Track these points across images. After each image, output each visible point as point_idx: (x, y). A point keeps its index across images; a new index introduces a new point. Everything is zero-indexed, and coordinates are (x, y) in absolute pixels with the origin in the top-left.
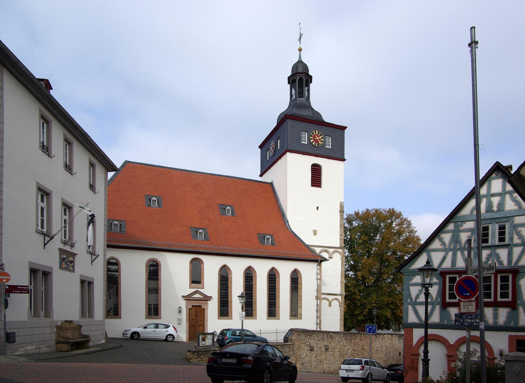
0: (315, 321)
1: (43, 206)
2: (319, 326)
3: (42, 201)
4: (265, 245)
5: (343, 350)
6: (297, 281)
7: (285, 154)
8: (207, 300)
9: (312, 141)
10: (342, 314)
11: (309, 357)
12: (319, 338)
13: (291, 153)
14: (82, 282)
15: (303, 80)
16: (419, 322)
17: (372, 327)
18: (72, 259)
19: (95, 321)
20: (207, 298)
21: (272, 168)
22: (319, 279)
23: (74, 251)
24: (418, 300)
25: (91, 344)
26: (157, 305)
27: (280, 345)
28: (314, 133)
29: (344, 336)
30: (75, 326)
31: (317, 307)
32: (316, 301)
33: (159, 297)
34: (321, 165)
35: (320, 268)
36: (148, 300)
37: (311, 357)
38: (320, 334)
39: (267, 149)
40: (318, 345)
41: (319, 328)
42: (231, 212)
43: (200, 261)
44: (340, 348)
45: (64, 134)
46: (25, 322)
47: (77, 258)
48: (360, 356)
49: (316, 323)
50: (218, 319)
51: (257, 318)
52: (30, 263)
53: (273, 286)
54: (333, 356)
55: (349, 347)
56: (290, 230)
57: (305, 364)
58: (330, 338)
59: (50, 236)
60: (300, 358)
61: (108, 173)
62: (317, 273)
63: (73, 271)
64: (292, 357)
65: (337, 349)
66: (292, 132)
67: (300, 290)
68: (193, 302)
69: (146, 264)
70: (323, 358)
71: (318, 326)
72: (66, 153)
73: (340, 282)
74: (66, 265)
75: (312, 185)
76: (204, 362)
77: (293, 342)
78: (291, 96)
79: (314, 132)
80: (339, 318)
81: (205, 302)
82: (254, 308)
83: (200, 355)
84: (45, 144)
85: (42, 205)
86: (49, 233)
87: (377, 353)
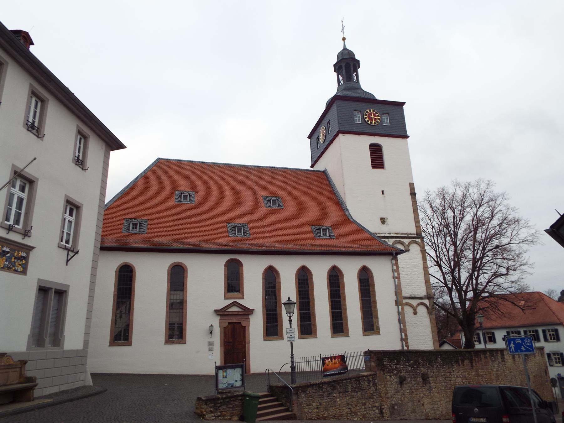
1: (71, 219)
2: (406, 343)
3: (71, 214)
5: (449, 379)
6: (368, 282)
7: (338, 136)
8: (249, 315)
13: (344, 134)
14: (43, 290)
15: (350, 65)
18: (24, 255)
19: (64, 351)
20: (247, 312)
22: (397, 278)
23: (27, 241)
25: (37, 393)
26: (182, 324)
28: (369, 112)
30: (12, 363)
31: (399, 316)
33: (184, 313)
34: (381, 144)
35: (395, 263)
36: (170, 317)
37: (404, 394)
39: (317, 137)
41: (406, 346)
43: (239, 264)
45: (78, 126)
46: (86, 356)
50: (264, 340)
51: (318, 337)
52: (39, 280)
54: (436, 389)
59: (74, 251)
62: (393, 270)
63: (24, 272)
67: (372, 294)
68: (229, 317)
69: (168, 270)
72: (80, 147)
73: (424, 281)
75: (372, 167)
78: (339, 82)
79: (368, 111)
81: (245, 317)
83: (219, 405)
84: (81, 158)
85: (69, 218)
86: (74, 248)
87: (499, 379)
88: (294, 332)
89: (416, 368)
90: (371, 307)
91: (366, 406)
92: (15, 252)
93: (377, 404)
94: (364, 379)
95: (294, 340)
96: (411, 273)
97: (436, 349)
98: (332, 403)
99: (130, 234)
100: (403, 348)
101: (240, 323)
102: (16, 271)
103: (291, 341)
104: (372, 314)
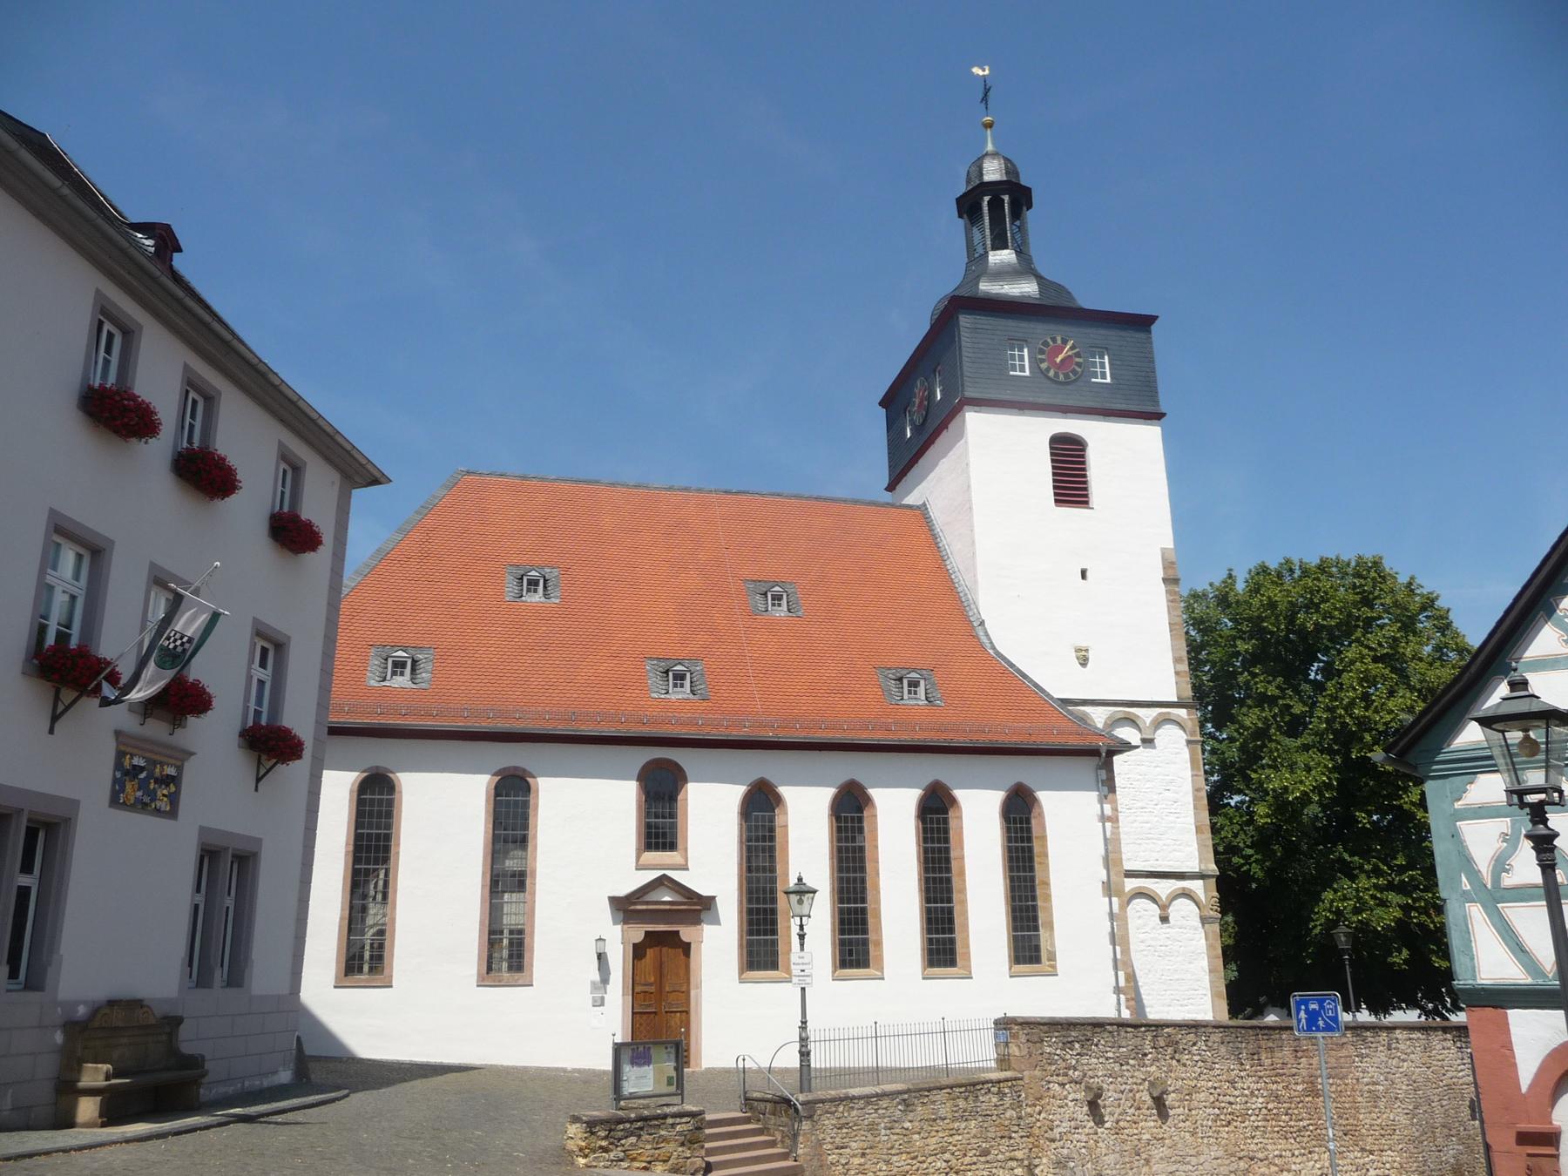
0: (1106, 977)
3: (263, 664)
4: (903, 707)
9: (1044, 366)
10: (1215, 949)
11: (1087, 1130)
12: (1122, 1050)
14: (209, 855)
15: (1004, 200)
16: (1529, 981)
17: (1322, 1007)
18: (171, 771)
20: (698, 907)
21: (921, 461)
22: (1109, 819)
24: (1508, 881)
27: (960, 1086)
29: (1228, 1039)
31: (1112, 924)
32: (1107, 899)
35: (1108, 779)
38: (1126, 1032)
40: (1119, 1079)
41: (1127, 1008)
42: (785, 602)
44: (1215, 1088)
47: (190, 769)
48: (1305, 1123)
49: (1112, 988)
52: (203, 830)
53: (940, 850)
55: (1249, 1083)
56: (991, 651)
57: (1072, 1164)
58: (1170, 1050)
60: (1046, 1135)
61: (351, 493)
63: (173, 814)
64: (1013, 1135)
65: (1203, 1094)
66: (976, 346)
67: (1040, 863)
70: (1145, 1137)
71: (1122, 997)
74: (139, 794)
75: (1056, 501)
76: (637, 1164)
77: (1015, 1070)
79: (1049, 340)
80: (1205, 963)
82: (871, 936)
83: (620, 1134)
88: (809, 964)
89: (1134, 1066)
90: (1034, 898)
91: (988, 1158)
92: (155, 767)
93: (1019, 1154)
94: (989, 1090)
95: (808, 984)
96: (1156, 805)
97: (1218, 1019)
98: (900, 1145)
99: (387, 688)
100: (1119, 1011)
101: (677, 933)
102: (158, 812)
103: (803, 986)
104: (1035, 919)
